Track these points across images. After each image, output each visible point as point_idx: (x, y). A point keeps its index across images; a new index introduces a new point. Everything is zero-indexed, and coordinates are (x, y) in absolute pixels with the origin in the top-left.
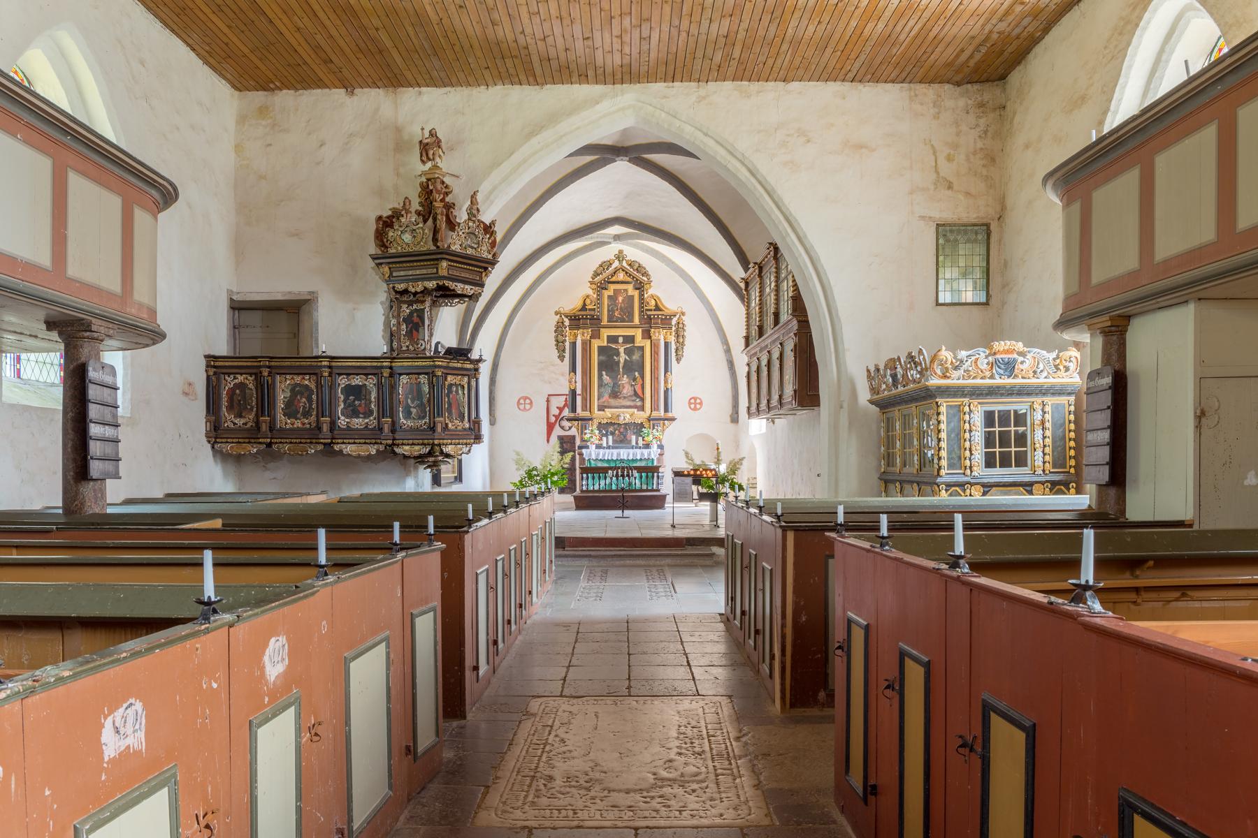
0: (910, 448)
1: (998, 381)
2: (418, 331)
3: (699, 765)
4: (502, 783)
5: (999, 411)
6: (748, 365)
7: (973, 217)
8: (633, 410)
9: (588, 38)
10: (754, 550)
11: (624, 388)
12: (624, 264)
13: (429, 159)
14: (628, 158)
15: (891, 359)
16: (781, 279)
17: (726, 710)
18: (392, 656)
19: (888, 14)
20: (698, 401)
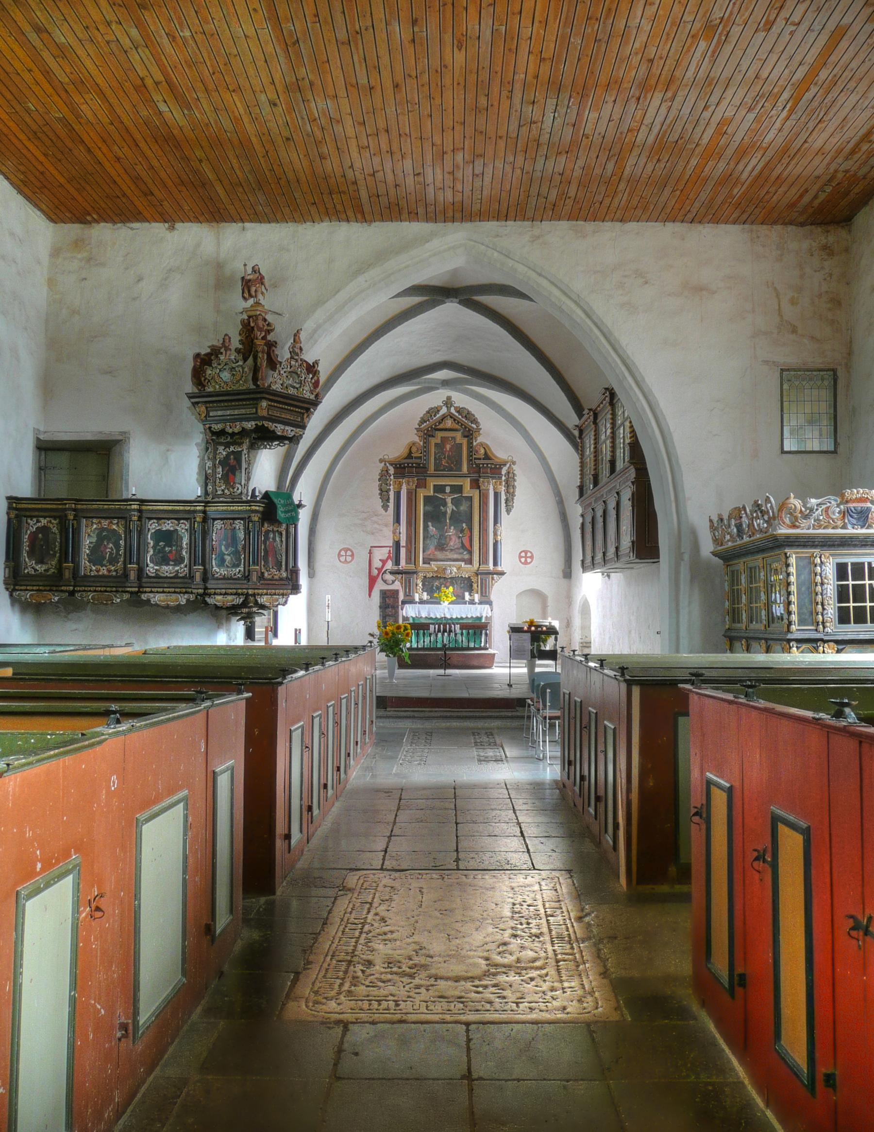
0: (756, 603)
1: (850, 531)
2: (234, 475)
3: (538, 949)
4: (315, 968)
5: (852, 564)
6: (582, 516)
7: (818, 362)
8: (460, 563)
9: (419, 174)
10: (595, 708)
11: (450, 539)
12: (453, 410)
13: (251, 296)
14: (458, 300)
15: (735, 508)
16: (617, 425)
17: (565, 887)
18: (190, 819)
20: (529, 555)
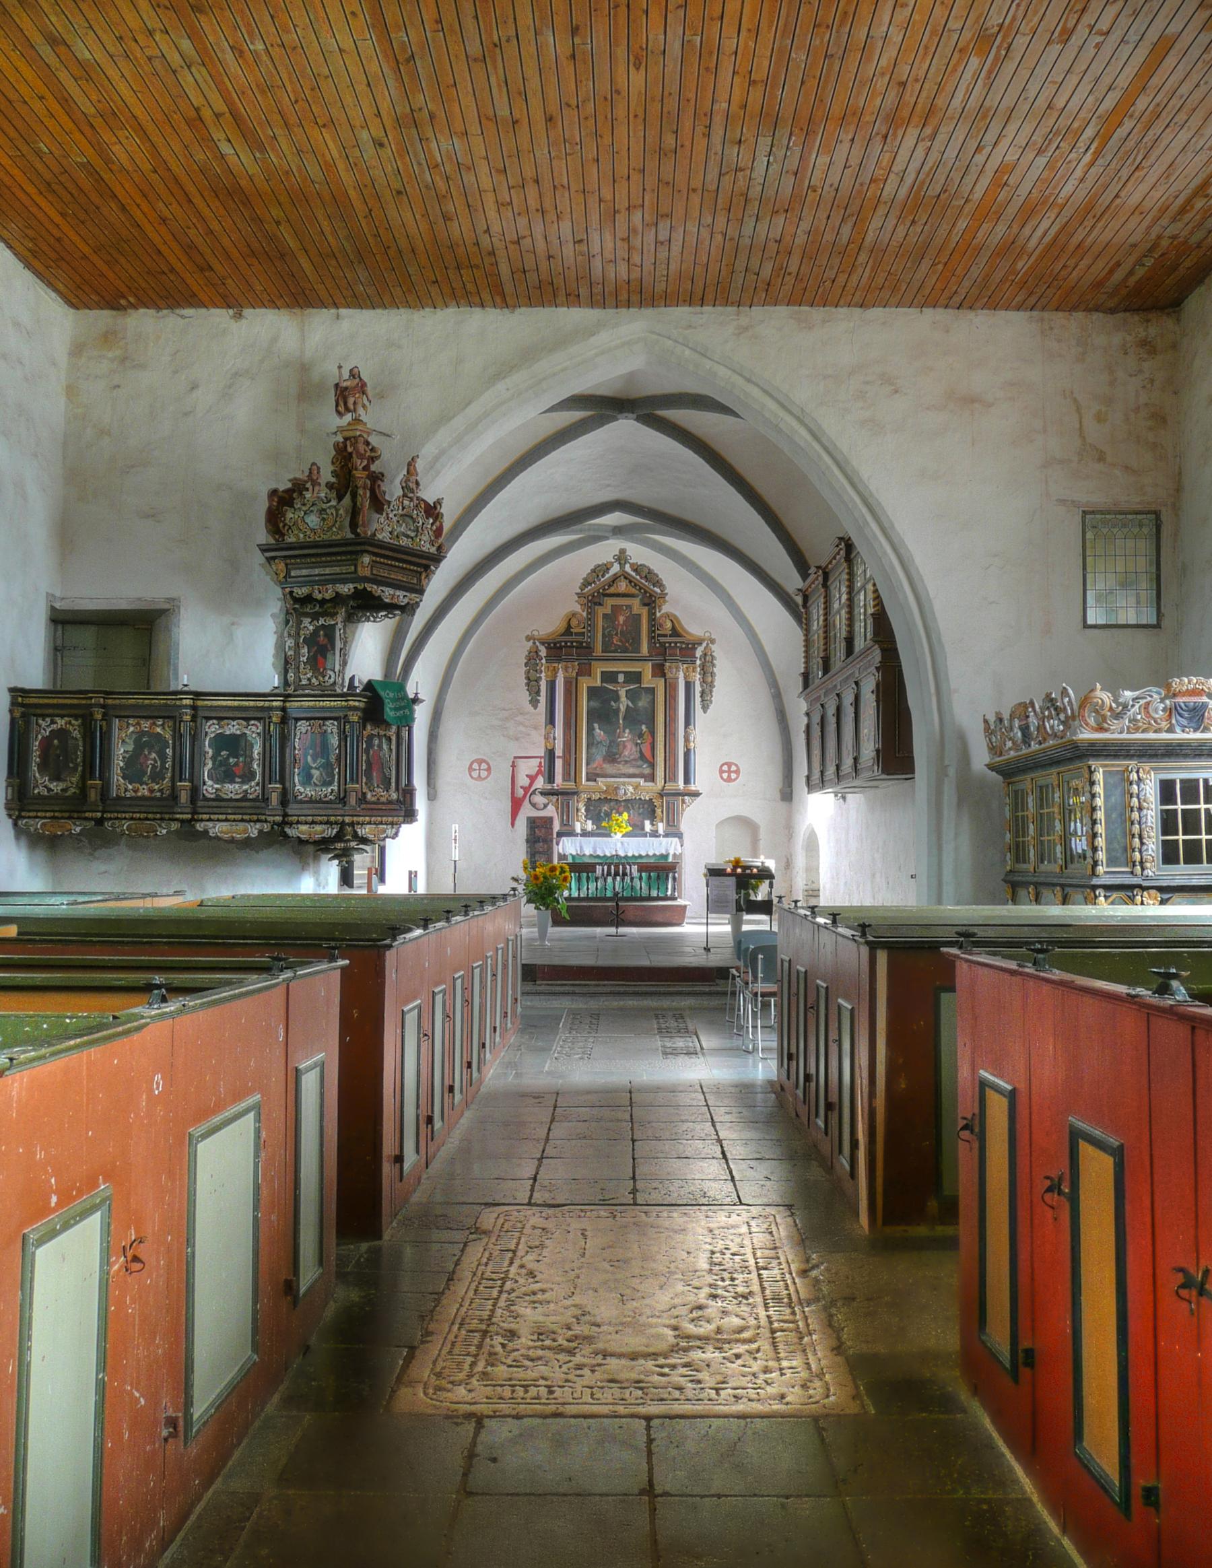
0: (1049, 835)
1: (1179, 735)
2: (325, 657)
3: (746, 1315)
4: (437, 1341)
5: (1182, 781)
6: (807, 714)
7: (1134, 501)
8: (638, 780)
9: (581, 241)
10: (825, 981)
11: (625, 747)
12: (628, 568)
13: (347, 410)
14: (635, 416)
15: (1020, 704)
16: (856, 589)
17: (783, 1229)
18: (264, 1135)
19: (1011, 210)
20: (733, 768)
